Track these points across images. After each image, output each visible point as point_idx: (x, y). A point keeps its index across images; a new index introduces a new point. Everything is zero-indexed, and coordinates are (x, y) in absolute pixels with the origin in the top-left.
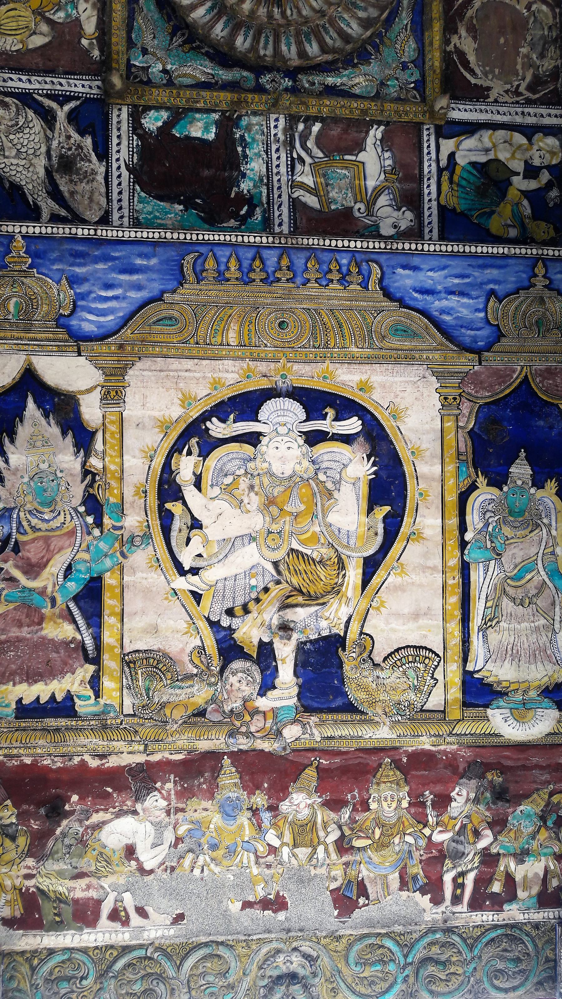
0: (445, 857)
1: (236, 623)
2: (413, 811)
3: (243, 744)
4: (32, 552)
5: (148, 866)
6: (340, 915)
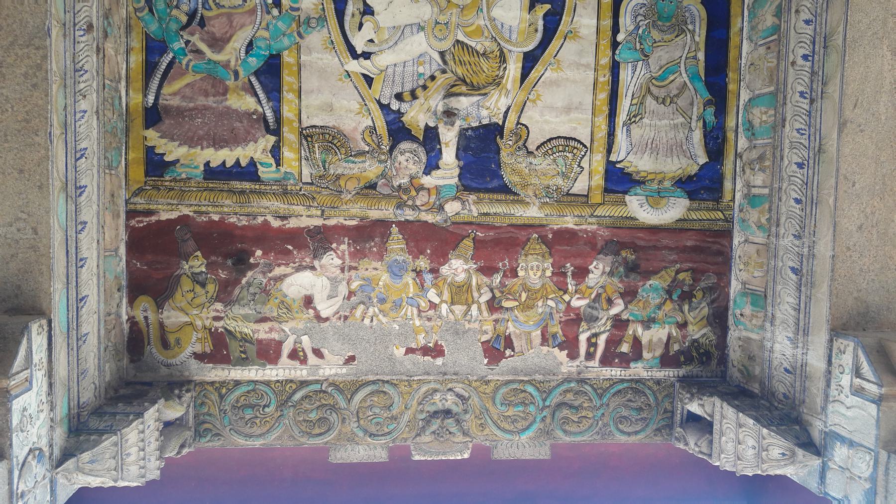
0: (581, 320)
1: (404, 107)
2: (555, 279)
3: (409, 215)
4: (217, 27)
5: (324, 314)
6: (489, 363)
